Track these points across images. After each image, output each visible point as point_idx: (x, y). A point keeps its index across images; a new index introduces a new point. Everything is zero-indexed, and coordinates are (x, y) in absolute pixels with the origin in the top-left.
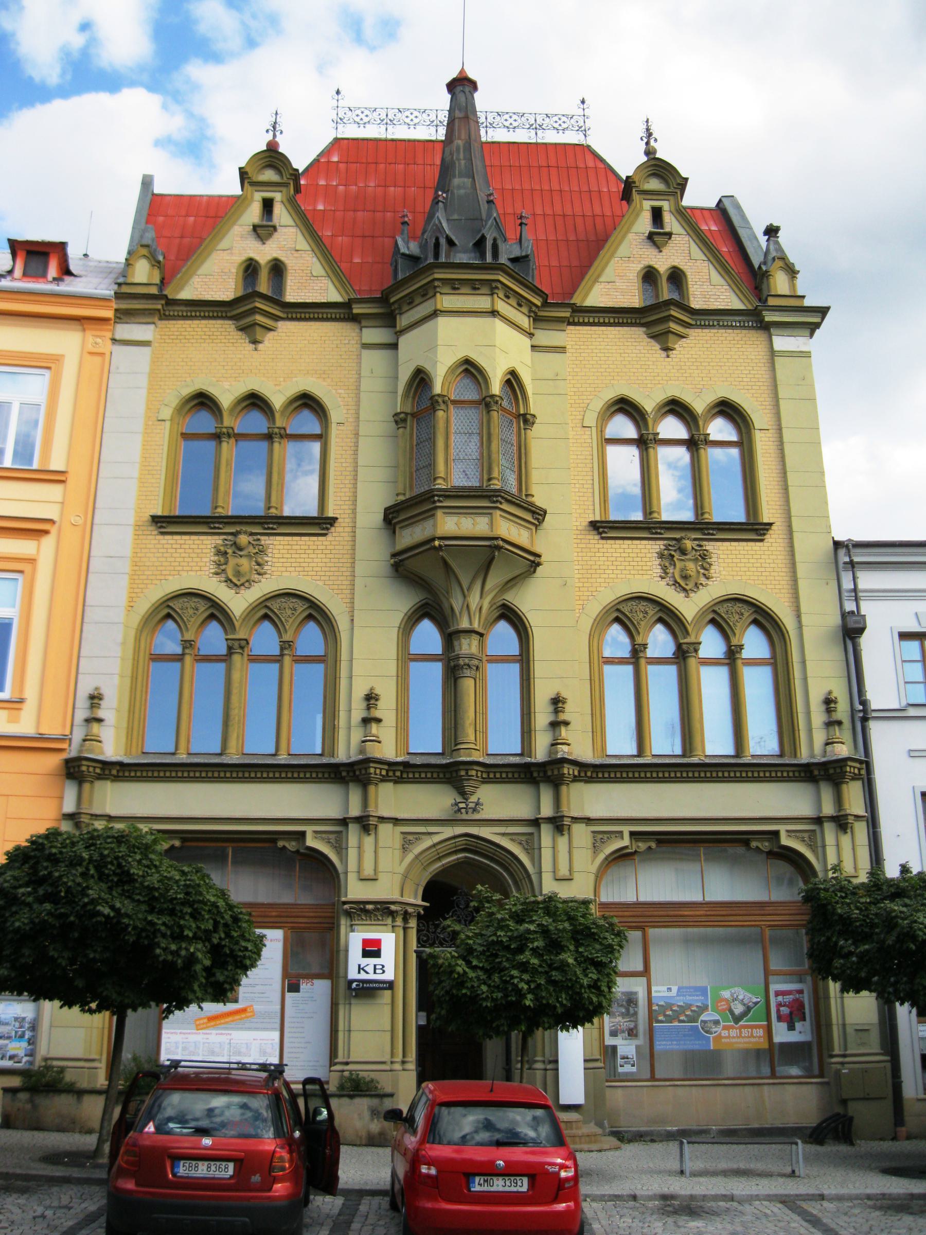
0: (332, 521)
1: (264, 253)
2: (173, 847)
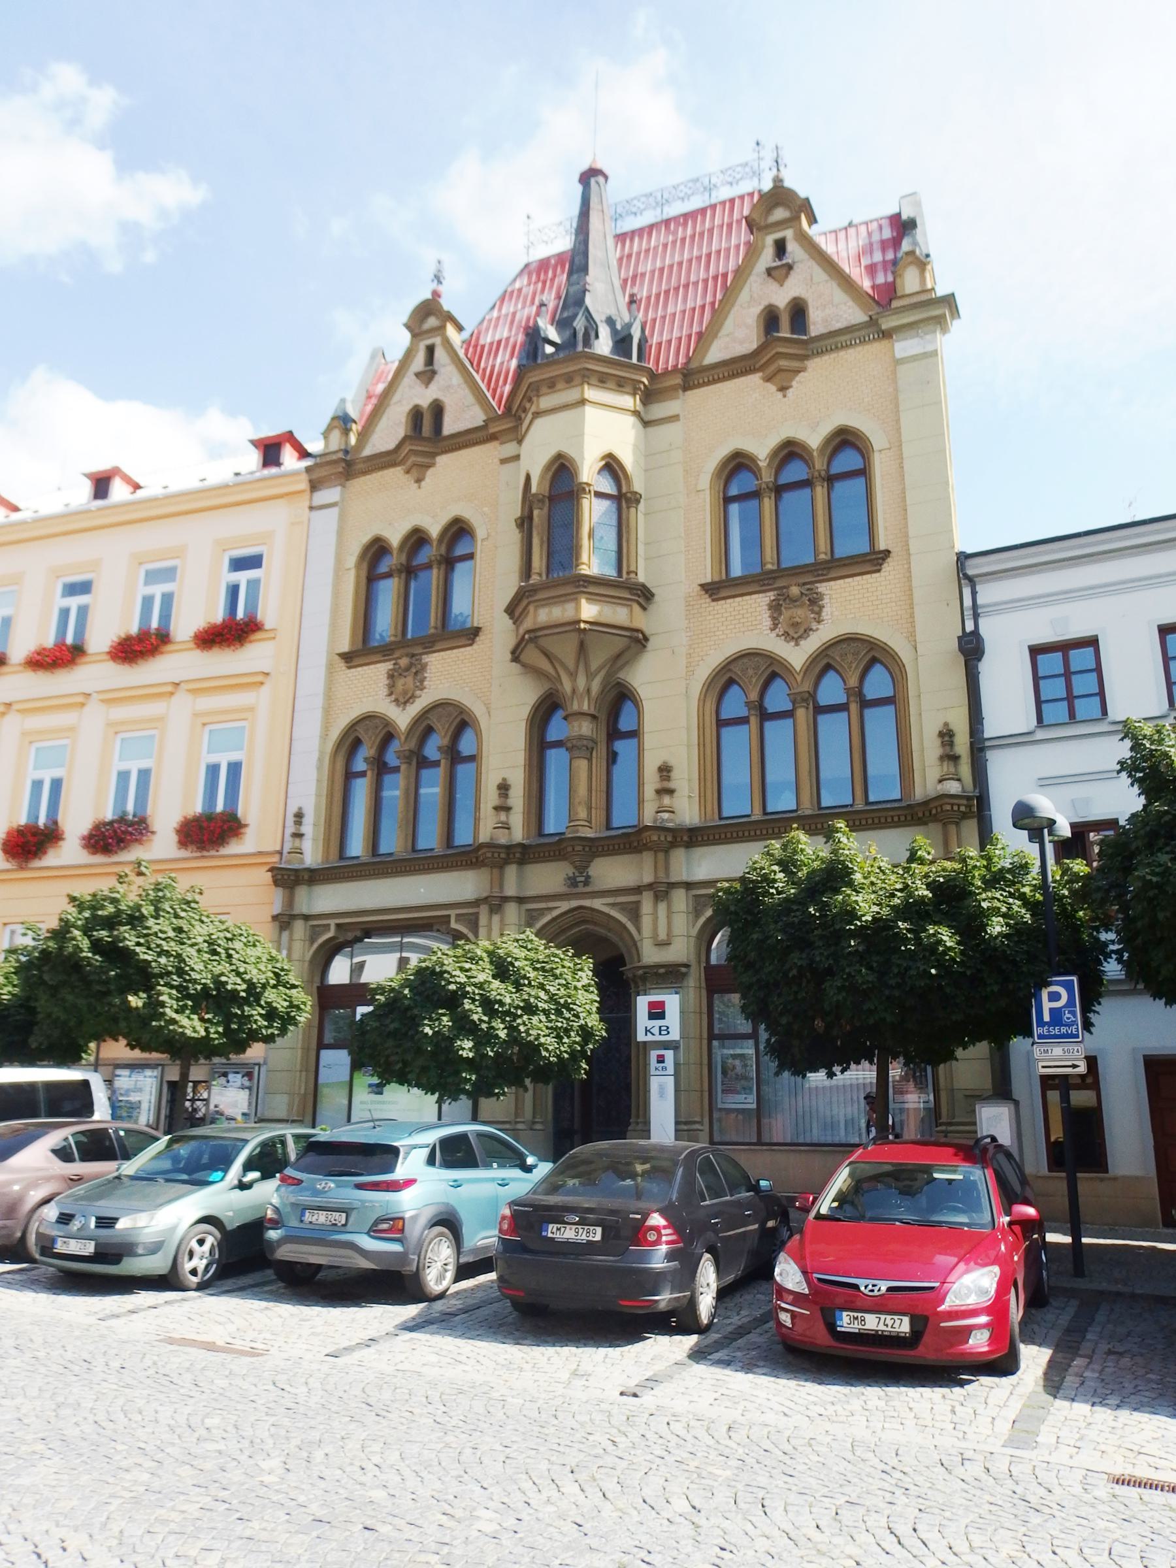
1: (781, 297)
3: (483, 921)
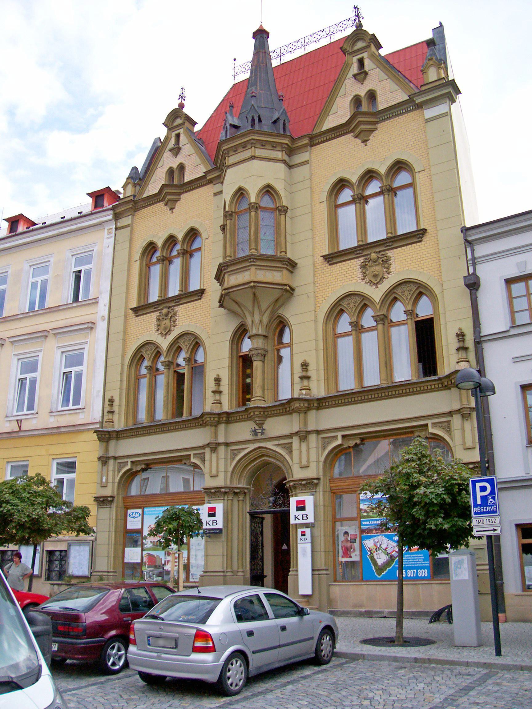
0: (423, 232)
1: (362, 91)
2: (356, 443)
3: (207, 456)
